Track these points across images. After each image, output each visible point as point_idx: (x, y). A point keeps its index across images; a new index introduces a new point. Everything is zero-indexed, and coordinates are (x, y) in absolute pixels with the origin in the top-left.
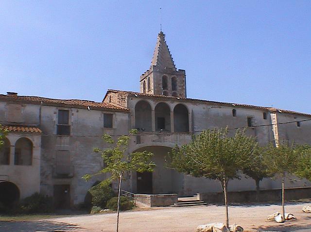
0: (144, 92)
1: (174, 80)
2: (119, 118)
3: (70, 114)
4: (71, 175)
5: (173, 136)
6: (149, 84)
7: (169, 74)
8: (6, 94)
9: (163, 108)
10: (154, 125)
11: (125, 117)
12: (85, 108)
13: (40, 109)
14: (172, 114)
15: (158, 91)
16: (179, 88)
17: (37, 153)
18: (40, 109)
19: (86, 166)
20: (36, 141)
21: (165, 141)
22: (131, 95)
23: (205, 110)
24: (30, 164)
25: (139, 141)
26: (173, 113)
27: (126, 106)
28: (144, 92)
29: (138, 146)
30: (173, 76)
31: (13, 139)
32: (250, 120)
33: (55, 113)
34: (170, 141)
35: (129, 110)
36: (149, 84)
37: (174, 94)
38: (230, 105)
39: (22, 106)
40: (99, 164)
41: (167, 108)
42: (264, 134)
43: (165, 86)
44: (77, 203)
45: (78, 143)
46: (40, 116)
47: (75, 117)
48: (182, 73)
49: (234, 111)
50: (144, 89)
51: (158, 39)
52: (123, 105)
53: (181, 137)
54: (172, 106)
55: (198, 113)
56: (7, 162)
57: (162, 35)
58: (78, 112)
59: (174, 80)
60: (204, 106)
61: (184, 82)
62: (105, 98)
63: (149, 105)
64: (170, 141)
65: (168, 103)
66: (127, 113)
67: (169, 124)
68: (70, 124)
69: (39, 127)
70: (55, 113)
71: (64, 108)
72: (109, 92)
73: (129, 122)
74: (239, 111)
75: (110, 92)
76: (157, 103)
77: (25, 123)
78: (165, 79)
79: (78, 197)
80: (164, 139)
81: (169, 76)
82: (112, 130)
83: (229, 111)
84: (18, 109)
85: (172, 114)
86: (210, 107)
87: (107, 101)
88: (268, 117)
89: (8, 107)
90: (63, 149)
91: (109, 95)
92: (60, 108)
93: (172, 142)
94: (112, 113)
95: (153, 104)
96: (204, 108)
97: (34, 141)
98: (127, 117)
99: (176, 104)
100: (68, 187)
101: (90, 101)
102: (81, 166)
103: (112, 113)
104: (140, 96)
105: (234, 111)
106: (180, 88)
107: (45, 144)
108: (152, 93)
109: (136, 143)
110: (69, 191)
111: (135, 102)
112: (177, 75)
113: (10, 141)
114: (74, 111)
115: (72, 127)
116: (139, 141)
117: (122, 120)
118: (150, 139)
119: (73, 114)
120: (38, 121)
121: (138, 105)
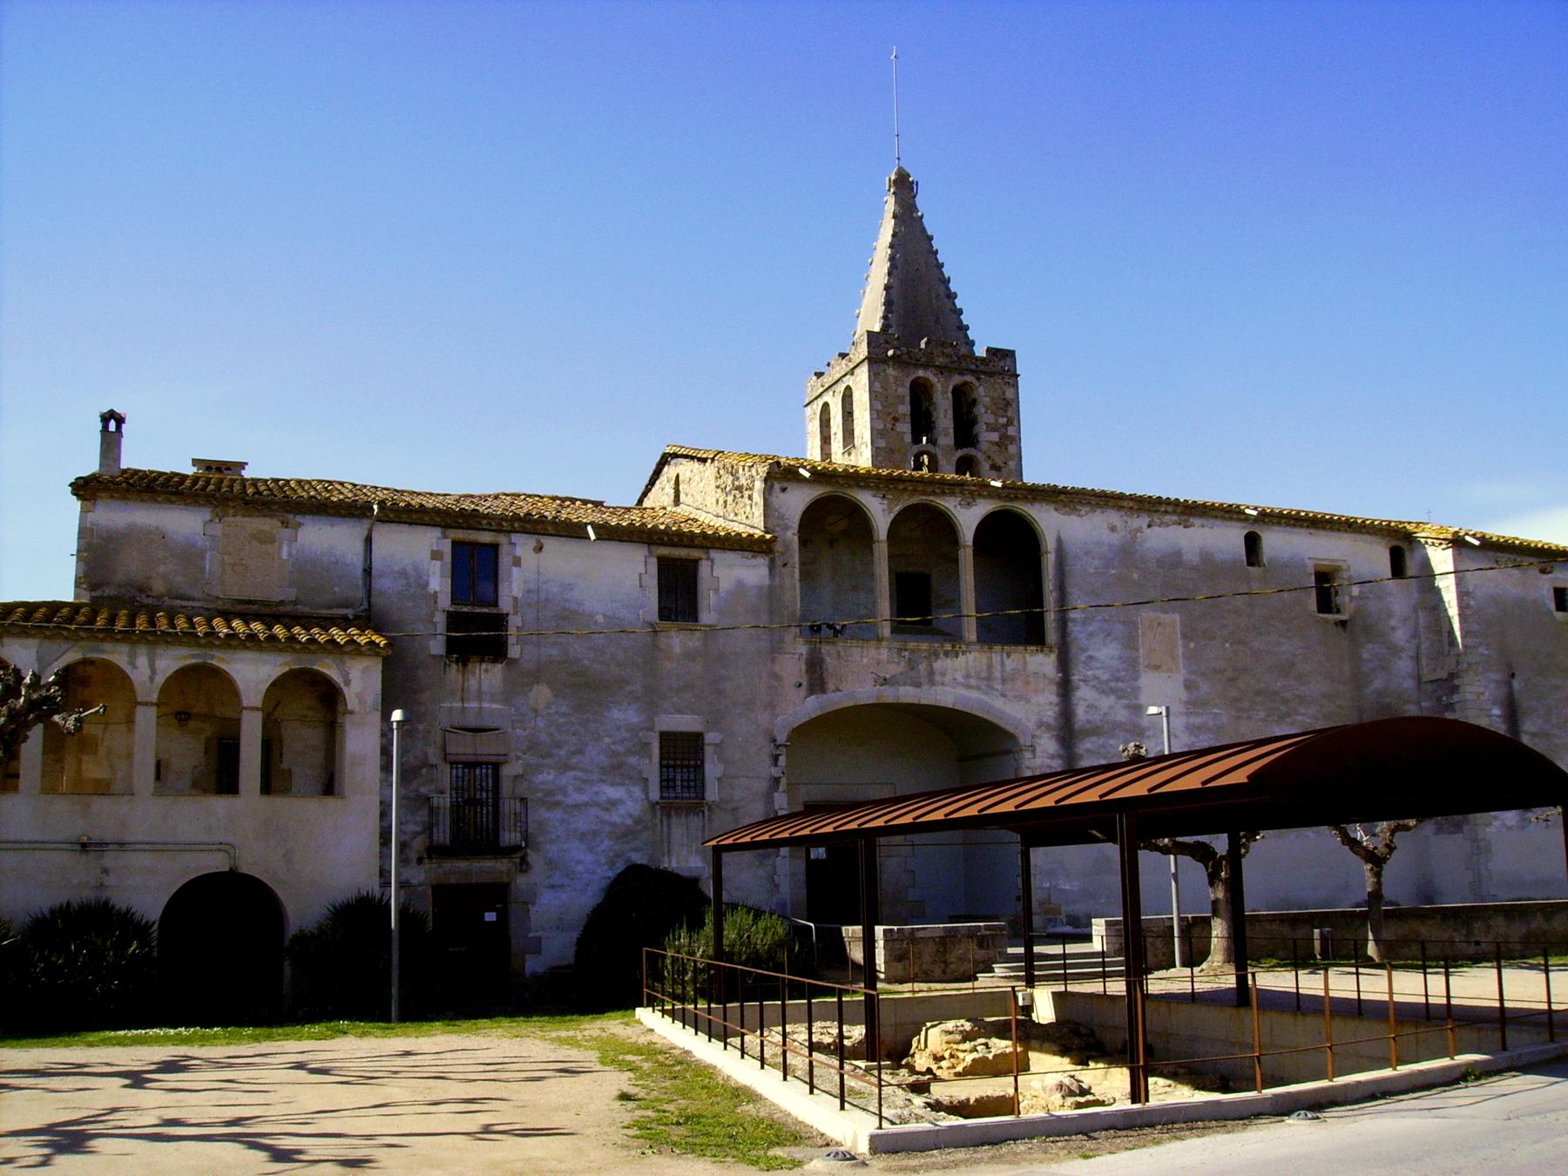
0: (826, 453)
1: (963, 403)
2: (725, 577)
3: (505, 560)
4: (509, 837)
5: (972, 660)
6: (848, 414)
7: (941, 370)
8: (190, 470)
9: (925, 527)
10: (885, 607)
11: (753, 572)
12: (574, 531)
13: (368, 541)
14: (966, 557)
15: (892, 451)
16: (987, 437)
17: (360, 742)
18: (368, 541)
19: (582, 798)
20: (360, 682)
21: (938, 678)
22: (781, 475)
23: (1115, 539)
24: (329, 787)
25: (816, 678)
26: (970, 551)
27: (758, 519)
28: (826, 453)
29: (810, 707)
30: (957, 379)
31: (253, 674)
32: (1325, 583)
33: (436, 555)
34: (963, 678)
35: (774, 540)
36: (848, 414)
37: (966, 464)
38: (1231, 513)
39: (285, 524)
40: (637, 791)
41: (945, 527)
42: (1395, 651)
43: (922, 422)
44: (540, 970)
45: (541, 694)
46: (368, 571)
47: (526, 571)
48: (1001, 364)
49: (1252, 542)
50: (826, 440)
51: (494, 725)
52: (741, 518)
53: (1010, 664)
54: (968, 517)
55: (1087, 553)
56: (224, 780)
57: (904, 186)
58: (539, 549)
59: (963, 403)
60: (1113, 517)
61: (1008, 407)
62: (652, 482)
63: (858, 514)
64: (963, 678)
65: (949, 504)
66: (762, 552)
67: (953, 602)
68: (505, 605)
69: (368, 619)
70: (436, 555)
71: (477, 539)
72: (665, 460)
73: (772, 594)
74: (1274, 542)
75: (675, 456)
76: (898, 509)
77: (295, 603)
78: (920, 395)
79: (558, 897)
80: (931, 673)
81: (938, 372)
82: (698, 634)
83: (1230, 539)
84: (270, 539)
85: (966, 557)
86: (1141, 521)
87: (661, 496)
88: (1411, 567)
89: (217, 529)
90: (473, 723)
91: (669, 472)
92: (461, 535)
93: (968, 687)
94: (695, 553)
95: (880, 512)
96: (1113, 529)
97: (348, 683)
98: (765, 571)
99: (983, 508)
100: (498, 894)
101: (585, 502)
102: (560, 797)
103: (695, 553)
104: (821, 476)
105: (1252, 542)
106: (995, 437)
107: (399, 685)
108: (863, 459)
109: (803, 691)
110: (503, 916)
111: (796, 501)
112: (976, 373)
113: (241, 686)
114: (523, 546)
115: (514, 621)
116: (816, 678)
117: (740, 584)
118: (870, 672)
119: (517, 562)
120: (361, 594)
121: (813, 517)
